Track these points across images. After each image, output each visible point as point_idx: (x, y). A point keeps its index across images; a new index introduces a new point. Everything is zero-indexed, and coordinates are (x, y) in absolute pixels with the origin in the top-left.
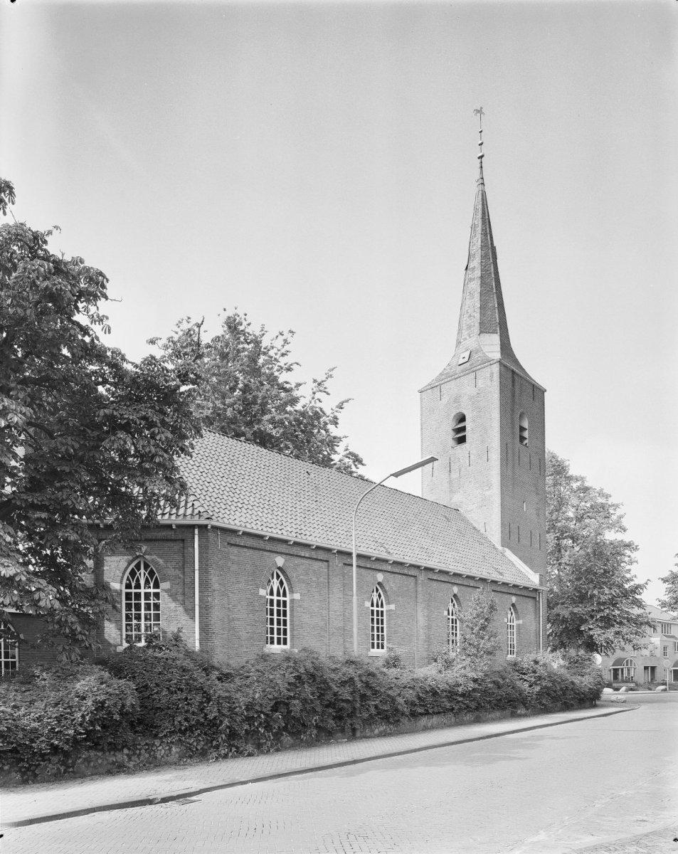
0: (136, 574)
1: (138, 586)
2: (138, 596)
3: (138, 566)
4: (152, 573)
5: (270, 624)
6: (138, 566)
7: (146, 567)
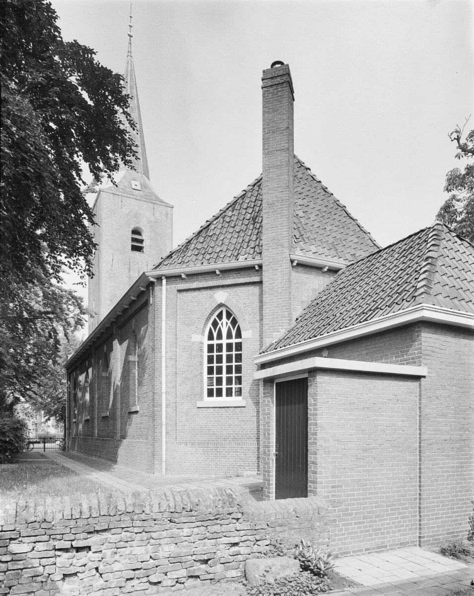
0: (218, 324)
1: (220, 336)
2: (220, 347)
3: (220, 316)
4: (234, 322)
5: (236, 373)
6: (220, 316)
7: (229, 315)
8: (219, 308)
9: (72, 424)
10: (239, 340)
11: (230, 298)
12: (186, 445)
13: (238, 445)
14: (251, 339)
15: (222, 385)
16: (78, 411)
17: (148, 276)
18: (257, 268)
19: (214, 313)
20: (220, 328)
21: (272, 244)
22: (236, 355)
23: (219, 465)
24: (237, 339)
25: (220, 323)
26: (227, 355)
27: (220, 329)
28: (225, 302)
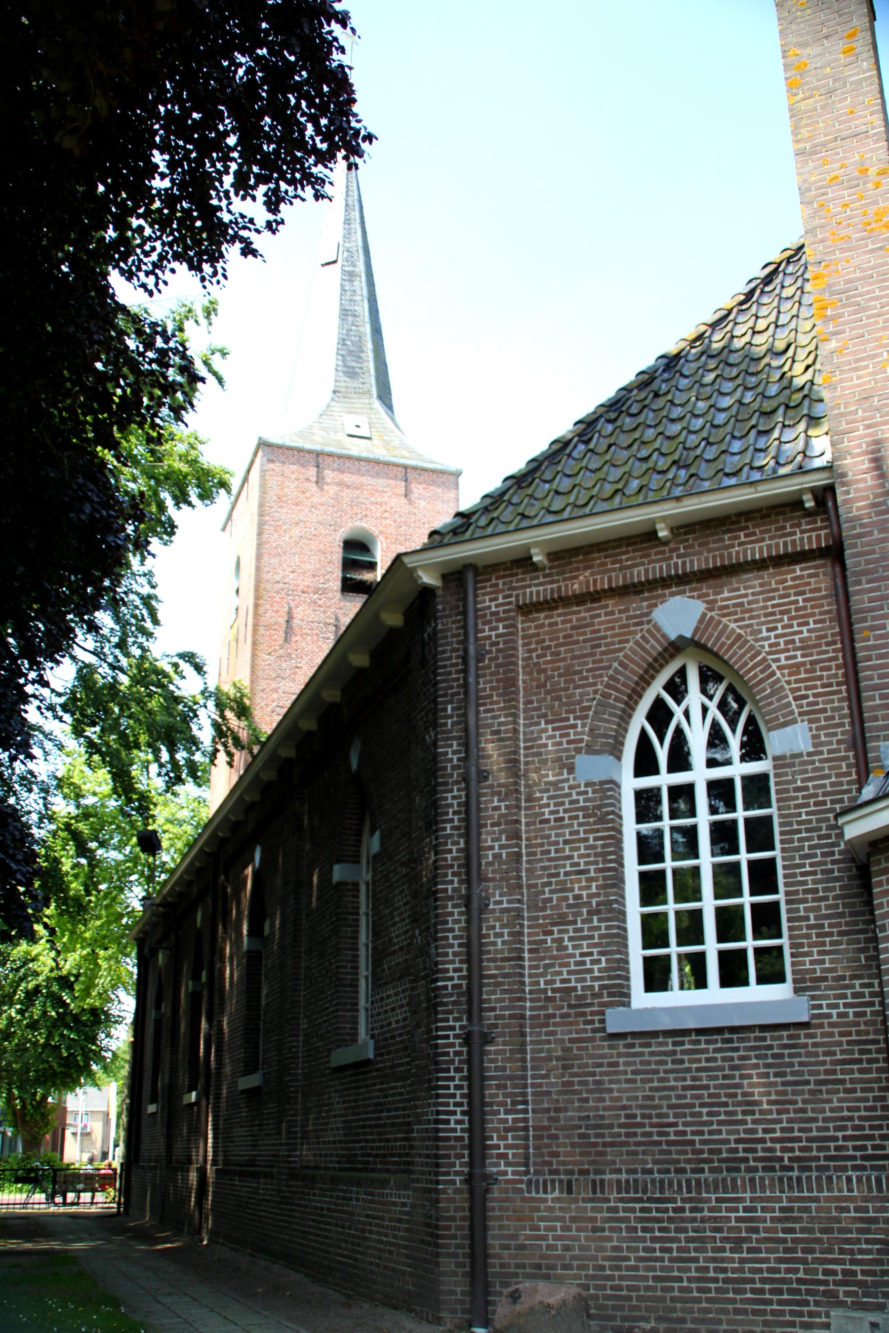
0: (670, 714)
3: (677, 689)
8: (672, 657)
9: (145, 1121)
10: (754, 767)
11: (712, 618)
12: (570, 1192)
13: (791, 1188)
14: (809, 754)
15: (701, 942)
16: (140, 957)
17: (414, 569)
18: (810, 504)
19: (653, 677)
20: (679, 732)
21: (864, 411)
22: (759, 952)
23: (716, 1280)
24: (744, 764)
25: (678, 711)
26: (722, 954)
27: (679, 733)
28: (694, 634)
